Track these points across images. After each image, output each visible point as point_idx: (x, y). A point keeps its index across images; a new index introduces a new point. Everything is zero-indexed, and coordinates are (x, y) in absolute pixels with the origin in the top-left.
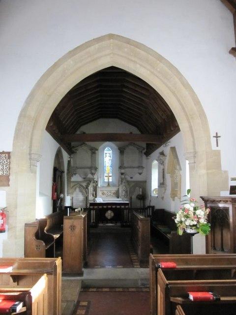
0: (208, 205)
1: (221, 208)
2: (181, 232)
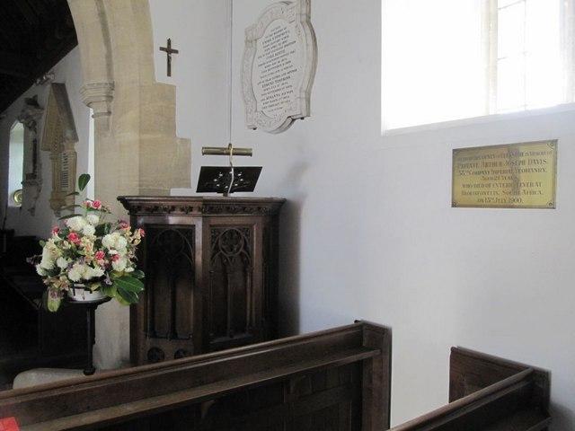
0: (141, 221)
1: (173, 228)
2: (54, 303)
